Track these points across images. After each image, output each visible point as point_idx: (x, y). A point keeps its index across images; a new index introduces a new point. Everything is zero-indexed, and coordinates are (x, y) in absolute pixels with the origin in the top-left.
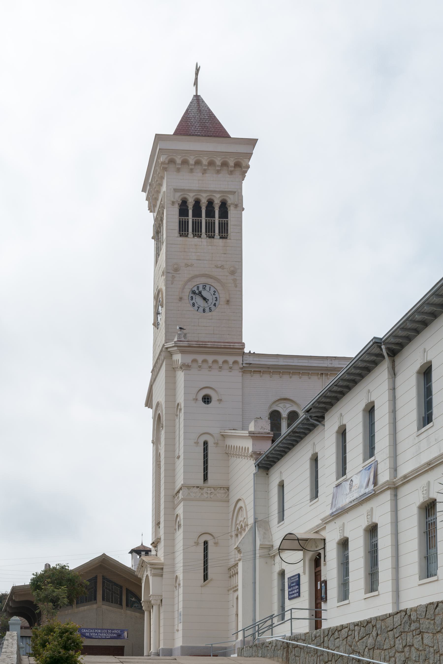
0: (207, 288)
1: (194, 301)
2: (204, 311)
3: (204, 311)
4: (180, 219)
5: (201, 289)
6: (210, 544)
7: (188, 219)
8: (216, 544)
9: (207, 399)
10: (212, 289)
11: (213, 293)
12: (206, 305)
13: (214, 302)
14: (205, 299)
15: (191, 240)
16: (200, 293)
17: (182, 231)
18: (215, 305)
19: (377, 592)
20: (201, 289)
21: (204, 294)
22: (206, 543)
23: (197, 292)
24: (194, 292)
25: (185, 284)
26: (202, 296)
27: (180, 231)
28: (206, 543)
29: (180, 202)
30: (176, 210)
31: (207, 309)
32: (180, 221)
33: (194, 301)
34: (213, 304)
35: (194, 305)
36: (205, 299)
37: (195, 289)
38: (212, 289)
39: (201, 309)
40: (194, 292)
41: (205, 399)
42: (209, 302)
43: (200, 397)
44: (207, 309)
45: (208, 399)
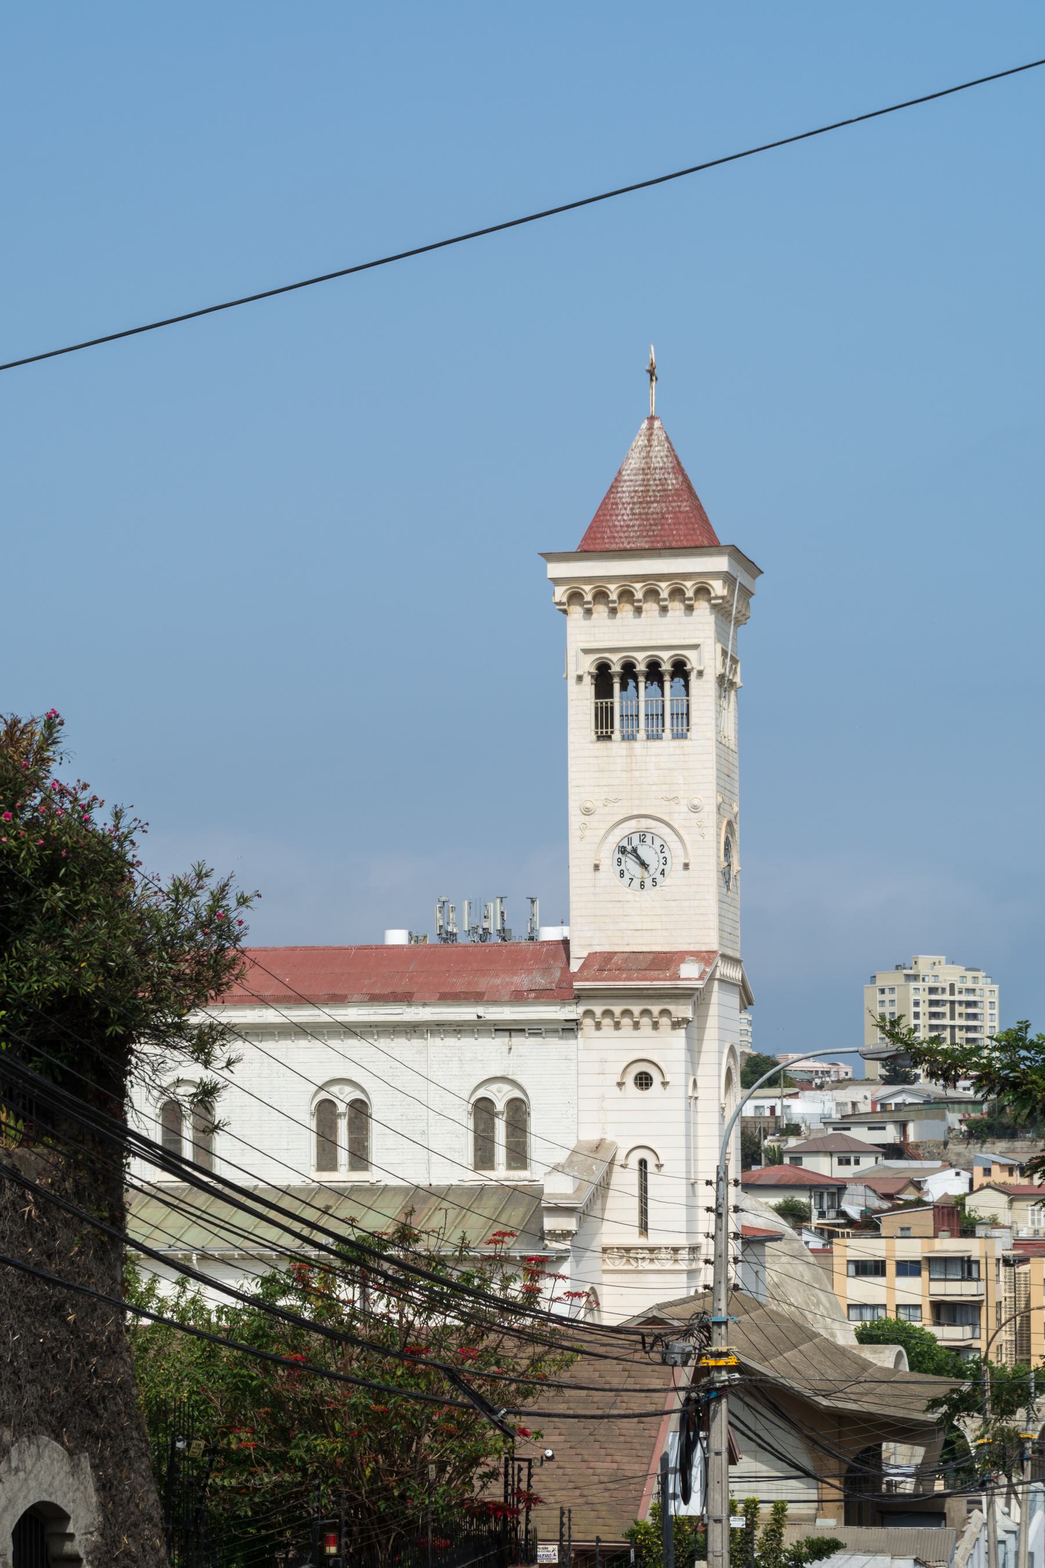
0: (648, 839)
1: (623, 867)
2: (642, 885)
3: (642, 885)
4: (596, 703)
5: (636, 842)
6: (651, 1167)
7: (612, 703)
8: (659, 1166)
9: (644, 1081)
10: (658, 842)
11: (659, 849)
12: (646, 875)
13: (662, 867)
14: (643, 865)
15: (617, 746)
16: (635, 850)
17: (602, 728)
18: (663, 873)
19: (888, 1262)
20: (636, 842)
21: (642, 852)
22: (643, 1163)
23: (629, 848)
24: (623, 850)
25: (605, 837)
26: (638, 857)
27: (597, 727)
28: (643, 1163)
29: (593, 670)
30: (588, 688)
31: (648, 882)
32: (596, 708)
33: (623, 867)
34: (660, 870)
35: (622, 874)
36: (643, 865)
37: (625, 843)
38: (658, 842)
39: (636, 883)
40: (623, 850)
41: (641, 1079)
42: (651, 869)
43: (630, 1080)
44: (648, 882)
45: (646, 1079)
